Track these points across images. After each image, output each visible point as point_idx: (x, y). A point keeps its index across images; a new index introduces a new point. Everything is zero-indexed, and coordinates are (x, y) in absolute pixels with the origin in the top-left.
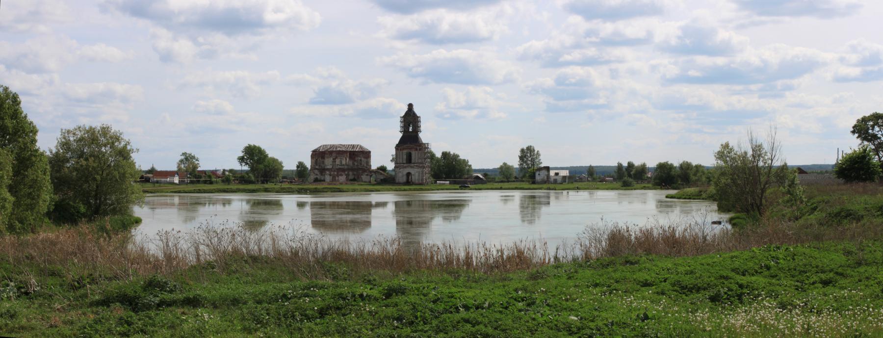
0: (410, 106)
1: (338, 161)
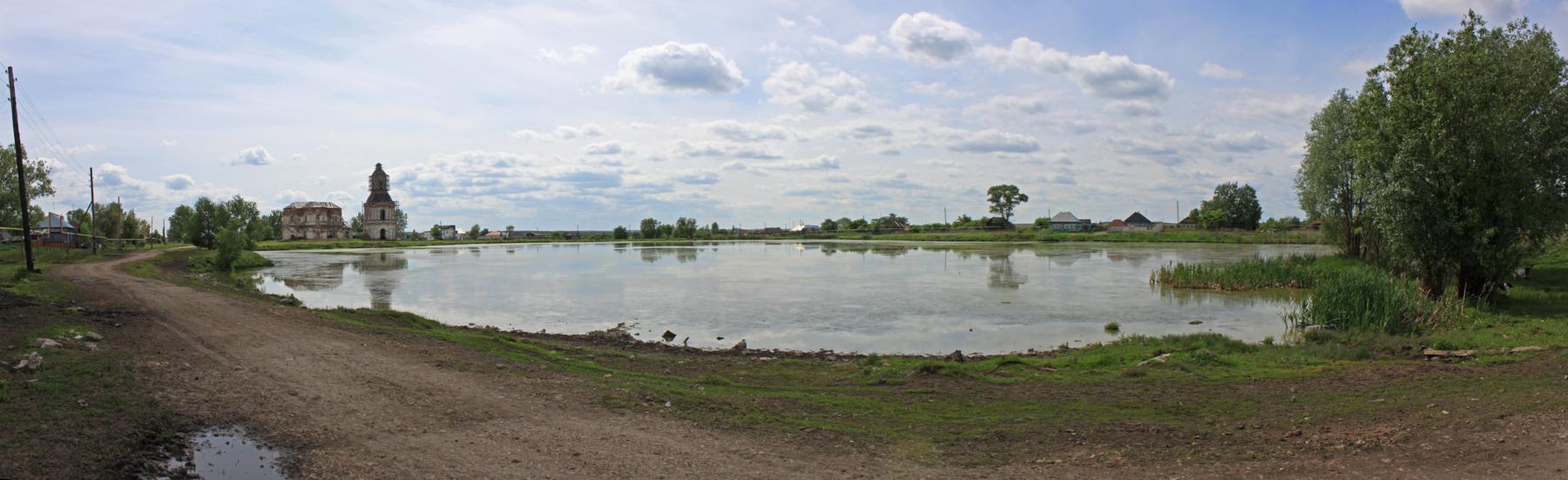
0: (379, 166)
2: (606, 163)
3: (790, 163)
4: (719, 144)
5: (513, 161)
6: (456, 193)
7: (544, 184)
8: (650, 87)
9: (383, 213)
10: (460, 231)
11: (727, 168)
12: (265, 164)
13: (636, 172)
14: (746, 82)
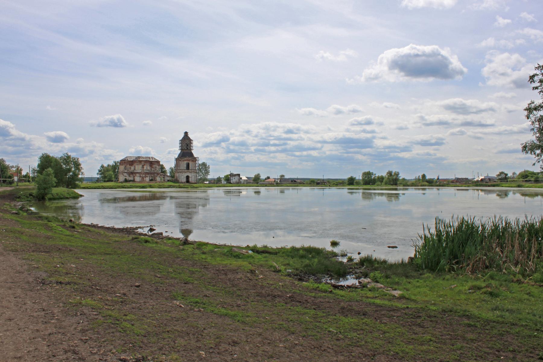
0: (186, 133)
1: (145, 167)
2: (364, 131)
3: (503, 128)
4: (448, 116)
5: (298, 130)
6: (257, 151)
7: (319, 145)
8: (396, 77)
9: (188, 165)
10: (244, 178)
11: (453, 134)
12: (121, 126)
13: (384, 138)
14: (465, 70)
